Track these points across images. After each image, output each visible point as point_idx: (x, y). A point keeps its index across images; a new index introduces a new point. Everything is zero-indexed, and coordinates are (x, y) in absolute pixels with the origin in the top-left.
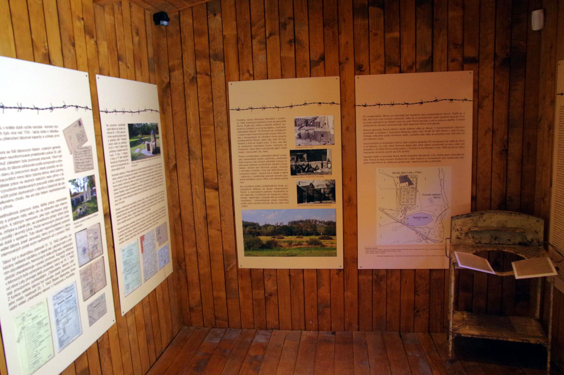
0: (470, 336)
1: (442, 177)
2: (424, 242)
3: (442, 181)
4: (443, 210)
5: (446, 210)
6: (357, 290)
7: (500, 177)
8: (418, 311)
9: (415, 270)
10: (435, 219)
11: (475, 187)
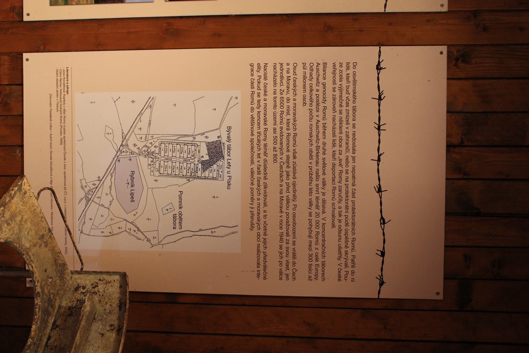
1: (220, 232)
2: (80, 194)
3: (209, 232)
4: (149, 235)
5: (149, 240)
10: (130, 217)
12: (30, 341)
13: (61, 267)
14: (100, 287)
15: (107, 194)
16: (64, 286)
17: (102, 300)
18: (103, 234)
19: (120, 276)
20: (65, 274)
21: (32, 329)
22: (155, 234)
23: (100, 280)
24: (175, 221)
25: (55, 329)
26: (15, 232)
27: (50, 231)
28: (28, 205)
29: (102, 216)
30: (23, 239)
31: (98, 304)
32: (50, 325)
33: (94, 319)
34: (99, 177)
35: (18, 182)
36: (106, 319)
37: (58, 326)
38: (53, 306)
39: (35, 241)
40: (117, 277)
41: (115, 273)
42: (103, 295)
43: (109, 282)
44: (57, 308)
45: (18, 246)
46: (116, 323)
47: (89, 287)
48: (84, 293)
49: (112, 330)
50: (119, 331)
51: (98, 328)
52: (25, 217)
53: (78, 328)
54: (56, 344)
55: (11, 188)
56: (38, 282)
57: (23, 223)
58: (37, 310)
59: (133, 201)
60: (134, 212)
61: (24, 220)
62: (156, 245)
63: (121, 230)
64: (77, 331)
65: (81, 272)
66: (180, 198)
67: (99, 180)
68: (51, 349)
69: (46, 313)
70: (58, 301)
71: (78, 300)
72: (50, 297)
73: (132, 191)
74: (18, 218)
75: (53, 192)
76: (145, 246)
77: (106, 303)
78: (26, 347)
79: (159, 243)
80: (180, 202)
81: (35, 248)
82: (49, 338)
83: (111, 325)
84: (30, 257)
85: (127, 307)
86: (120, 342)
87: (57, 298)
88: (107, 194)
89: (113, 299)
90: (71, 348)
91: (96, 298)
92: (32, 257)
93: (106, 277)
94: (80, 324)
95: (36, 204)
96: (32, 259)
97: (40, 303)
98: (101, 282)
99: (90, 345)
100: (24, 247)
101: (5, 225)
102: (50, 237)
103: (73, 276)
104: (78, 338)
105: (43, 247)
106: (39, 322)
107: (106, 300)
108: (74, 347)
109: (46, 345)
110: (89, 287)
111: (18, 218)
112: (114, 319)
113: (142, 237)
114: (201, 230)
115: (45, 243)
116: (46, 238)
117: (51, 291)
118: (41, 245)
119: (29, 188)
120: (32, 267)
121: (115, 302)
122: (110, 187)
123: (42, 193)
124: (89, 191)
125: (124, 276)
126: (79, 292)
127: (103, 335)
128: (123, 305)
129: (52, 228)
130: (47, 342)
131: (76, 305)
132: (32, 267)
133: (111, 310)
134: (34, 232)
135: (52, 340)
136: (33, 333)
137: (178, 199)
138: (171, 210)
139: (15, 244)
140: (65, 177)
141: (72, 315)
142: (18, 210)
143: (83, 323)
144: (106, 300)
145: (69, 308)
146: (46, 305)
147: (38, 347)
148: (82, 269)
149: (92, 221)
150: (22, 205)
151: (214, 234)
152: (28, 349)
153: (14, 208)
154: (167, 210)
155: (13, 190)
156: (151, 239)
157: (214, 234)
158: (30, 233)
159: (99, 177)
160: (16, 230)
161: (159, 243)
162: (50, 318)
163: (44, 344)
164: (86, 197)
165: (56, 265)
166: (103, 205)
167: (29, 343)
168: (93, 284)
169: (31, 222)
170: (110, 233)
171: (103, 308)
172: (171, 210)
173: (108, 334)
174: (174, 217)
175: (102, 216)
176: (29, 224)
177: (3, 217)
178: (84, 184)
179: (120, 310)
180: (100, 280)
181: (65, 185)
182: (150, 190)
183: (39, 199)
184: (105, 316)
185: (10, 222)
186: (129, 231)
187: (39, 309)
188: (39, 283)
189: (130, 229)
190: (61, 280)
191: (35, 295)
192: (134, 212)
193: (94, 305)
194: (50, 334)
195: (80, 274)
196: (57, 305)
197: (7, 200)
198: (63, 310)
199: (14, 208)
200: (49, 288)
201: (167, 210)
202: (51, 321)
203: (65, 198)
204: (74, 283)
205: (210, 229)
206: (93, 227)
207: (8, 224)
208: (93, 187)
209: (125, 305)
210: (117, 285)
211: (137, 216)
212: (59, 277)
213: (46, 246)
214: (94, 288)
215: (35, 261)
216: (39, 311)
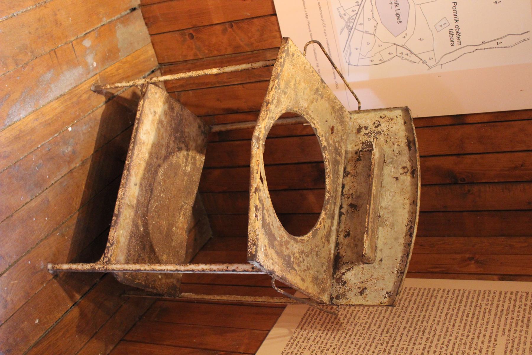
0: (138, 116)
1: (506, 42)
2: (340, 24)
3: (494, 44)
4: (425, 57)
5: (424, 62)
6: (289, 162)
7: (516, 168)
8: (192, 37)
9: (275, 14)
10: (400, 40)
11: (486, 119)
12: (327, 195)
13: (338, 111)
14: (382, 125)
15: (369, 19)
16: (346, 129)
17: (388, 140)
18: (373, 63)
19: (402, 110)
20: (344, 118)
21: (326, 183)
22: (431, 55)
23: (381, 117)
24: (452, 37)
25: (347, 176)
26: (292, 98)
27: (322, 81)
28: (298, 65)
29: (368, 44)
30: (301, 101)
31: (385, 146)
32: (341, 173)
33: (384, 162)
34: (357, 2)
35: (284, 47)
36: (396, 161)
37: (349, 173)
38: (339, 154)
39: (311, 98)
40: (399, 112)
41: (396, 108)
42: (388, 135)
43: (392, 119)
44: (344, 155)
45: (297, 109)
46: (408, 165)
47: (371, 127)
48: (367, 134)
49: (406, 172)
50: (413, 173)
51: (391, 172)
52: (298, 79)
53: (372, 179)
54: (351, 192)
55: (279, 56)
56: (322, 136)
57: (297, 85)
58: (327, 163)
59: (399, 22)
60: (403, 34)
61: (298, 82)
62: (434, 66)
63: (392, 56)
64: (372, 182)
65: (359, 111)
66: (455, 10)
67: (358, 5)
68: (348, 198)
69: (336, 163)
70: (343, 147)
71: (363, 143)
72: (336, 146)
73: (398, 12)
74: (292, 83)
75: (320, 45)
76: (422, 69)
77: (393, 143)
78: (325, 202)
79: (437, 64)
80: (456, 15)
81: (313, 104)
82: (343, 187)
83: (404, 168)
84: (310, 116)
85: (417, 146)
86: (417, 185)
87: (342, 144)
88: (369, 19)
89: (399, 138)
90: (370, 200)
91: (382, 138)
92: (312, 114)
93: (386, 113)
94: (373, 174)
95: (305, 61)
96: (312, 116)
97: (328, 157)
98: (383, 120)
99: (386, 191)
100: (303, 109)
101: (283, 96)
102: (324, 87)
103: (352, 116)
104: (374, 188)
105: (319, 100)
106: (331, 175)
107: (392, 140)
108: (372, 199)
109: (342, 194)
110: (371, 127)
111: (292, 83)
112: (405, 160)
113: (417, 60)
114: (484, 43)
115: (320, 95)
116: (321, 90)
117: (336, 140)
118: (317, 99)
119: (295, 48)
120: (314, 124)
121: (403, 142)
122: (372, 11)
123: (308, 47)
124: (349, 19)
125: (406, 110)
126: (362, 133)
127: (397, 179)
128: (411, 144)
129: (319, 70)
130: (342, 191)
131: (362, 148)
132: (314, 124)
133: (400, 150)
134: (308, 89)
135: (346, 188)
136: (328, 187)
137: (452, 12)
138: (446, 25)
139: (295, 109)
140: (320, 8)
141: (361, 160)
142: (290, 74)
143: (376, 171)
144: (392, 140)
145: (356, 153)
146: (334, 155)
147: (335, 199)
148: (359, 107)
149: (359, 50)
150: (293, 69)
151: (500, 45)
152: (328, 204)
153: (286, 75)
154: (441, 26)
155: (281, 58)
156: (427, 60)
157: (500, 45)
158: (305, 92)
159: (357, 2)
160: (293, 96)
161: (437, 64)
162: (340, 167)
163: (340, 194)
164: (347, 26)
165: (335, 112)
166: (367, 32)
167: (327, 198)
168: (375, 123)
169: (304, 81)
170: (381, 60)
171: (392, 149)
172: (446, 25)
173: (402, 178)
174: (451, 32)
175: (368, 44)
176: (303, 84)
177: (279, 89)
178: (342, 13)
179: (410, 149)
180: (381, 117)
181: (322, 16)
182: (418, 7)
183: (307, 54)
184: (395, 158)
185: (286, 90)
186: (400, 55)
187: (329, 162)
188: (324, 138)
189: (402, 53)
190: (341, 125)
191: (322, 149)
192: (403, 34)
193: (382, 149)
194: (343, 182)
195: (358, 113)
196: (343, 152)
197: (279, 71)
198: (350, 155)
199: (286, 75)
200: (333, 138)
201: (441, 26)
202: (342, 169)
203: (325, 30)
204: (355, 124)
205: (494, 40)
206: (361, 57)
207: (285, 93)
208: (352, 14)
209: (415, 145)
210: (401, 121)
211: (407, 38)
212: (340, 123)
213: (322, 98)
214: (376, 127)
215: (315, 118)
216: (329, 165)
